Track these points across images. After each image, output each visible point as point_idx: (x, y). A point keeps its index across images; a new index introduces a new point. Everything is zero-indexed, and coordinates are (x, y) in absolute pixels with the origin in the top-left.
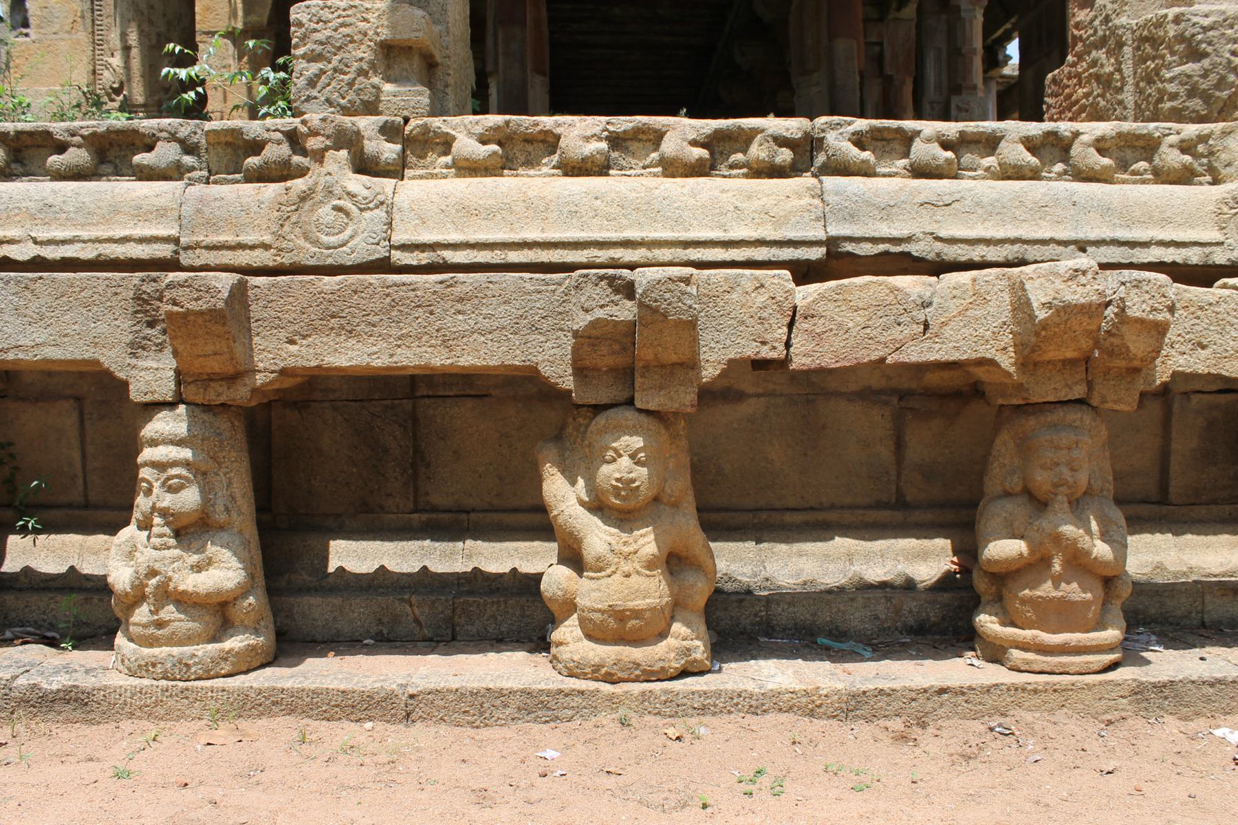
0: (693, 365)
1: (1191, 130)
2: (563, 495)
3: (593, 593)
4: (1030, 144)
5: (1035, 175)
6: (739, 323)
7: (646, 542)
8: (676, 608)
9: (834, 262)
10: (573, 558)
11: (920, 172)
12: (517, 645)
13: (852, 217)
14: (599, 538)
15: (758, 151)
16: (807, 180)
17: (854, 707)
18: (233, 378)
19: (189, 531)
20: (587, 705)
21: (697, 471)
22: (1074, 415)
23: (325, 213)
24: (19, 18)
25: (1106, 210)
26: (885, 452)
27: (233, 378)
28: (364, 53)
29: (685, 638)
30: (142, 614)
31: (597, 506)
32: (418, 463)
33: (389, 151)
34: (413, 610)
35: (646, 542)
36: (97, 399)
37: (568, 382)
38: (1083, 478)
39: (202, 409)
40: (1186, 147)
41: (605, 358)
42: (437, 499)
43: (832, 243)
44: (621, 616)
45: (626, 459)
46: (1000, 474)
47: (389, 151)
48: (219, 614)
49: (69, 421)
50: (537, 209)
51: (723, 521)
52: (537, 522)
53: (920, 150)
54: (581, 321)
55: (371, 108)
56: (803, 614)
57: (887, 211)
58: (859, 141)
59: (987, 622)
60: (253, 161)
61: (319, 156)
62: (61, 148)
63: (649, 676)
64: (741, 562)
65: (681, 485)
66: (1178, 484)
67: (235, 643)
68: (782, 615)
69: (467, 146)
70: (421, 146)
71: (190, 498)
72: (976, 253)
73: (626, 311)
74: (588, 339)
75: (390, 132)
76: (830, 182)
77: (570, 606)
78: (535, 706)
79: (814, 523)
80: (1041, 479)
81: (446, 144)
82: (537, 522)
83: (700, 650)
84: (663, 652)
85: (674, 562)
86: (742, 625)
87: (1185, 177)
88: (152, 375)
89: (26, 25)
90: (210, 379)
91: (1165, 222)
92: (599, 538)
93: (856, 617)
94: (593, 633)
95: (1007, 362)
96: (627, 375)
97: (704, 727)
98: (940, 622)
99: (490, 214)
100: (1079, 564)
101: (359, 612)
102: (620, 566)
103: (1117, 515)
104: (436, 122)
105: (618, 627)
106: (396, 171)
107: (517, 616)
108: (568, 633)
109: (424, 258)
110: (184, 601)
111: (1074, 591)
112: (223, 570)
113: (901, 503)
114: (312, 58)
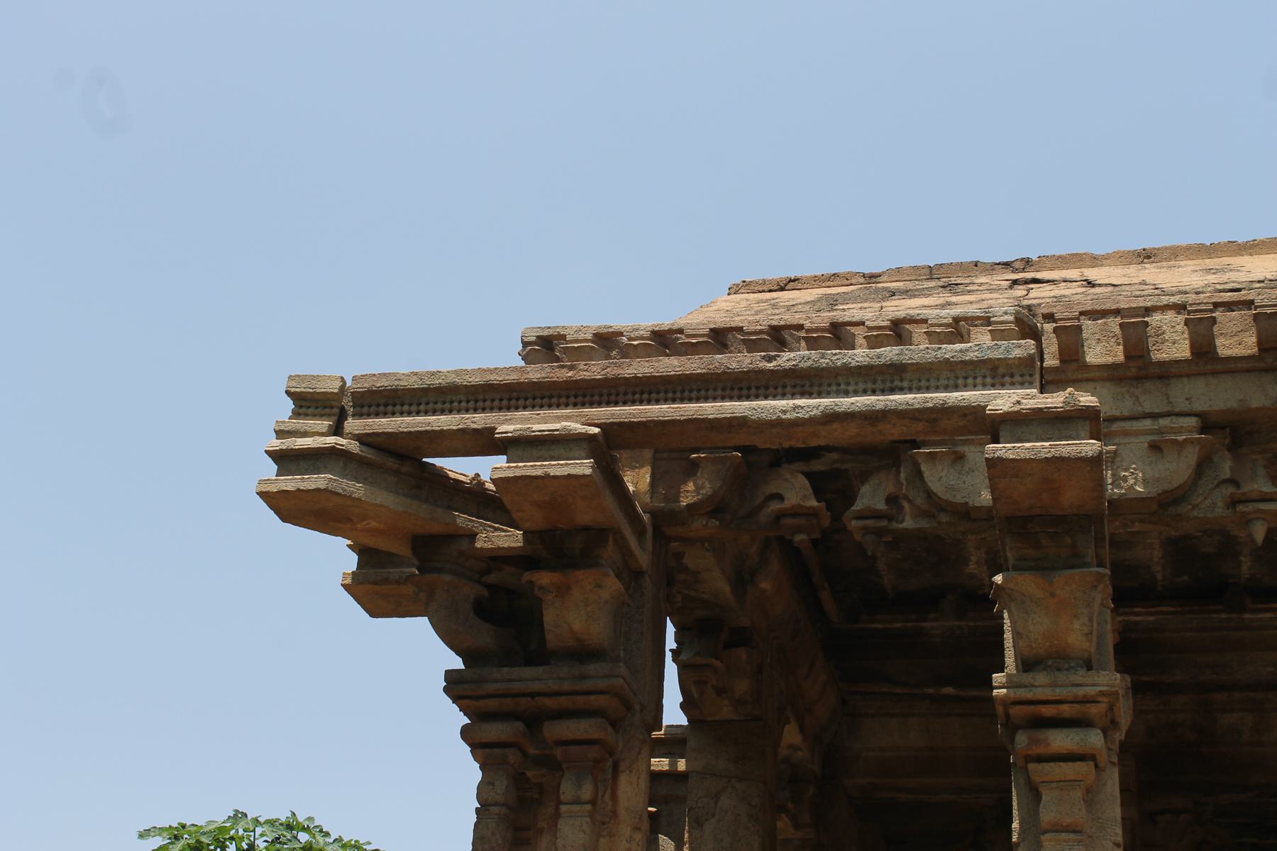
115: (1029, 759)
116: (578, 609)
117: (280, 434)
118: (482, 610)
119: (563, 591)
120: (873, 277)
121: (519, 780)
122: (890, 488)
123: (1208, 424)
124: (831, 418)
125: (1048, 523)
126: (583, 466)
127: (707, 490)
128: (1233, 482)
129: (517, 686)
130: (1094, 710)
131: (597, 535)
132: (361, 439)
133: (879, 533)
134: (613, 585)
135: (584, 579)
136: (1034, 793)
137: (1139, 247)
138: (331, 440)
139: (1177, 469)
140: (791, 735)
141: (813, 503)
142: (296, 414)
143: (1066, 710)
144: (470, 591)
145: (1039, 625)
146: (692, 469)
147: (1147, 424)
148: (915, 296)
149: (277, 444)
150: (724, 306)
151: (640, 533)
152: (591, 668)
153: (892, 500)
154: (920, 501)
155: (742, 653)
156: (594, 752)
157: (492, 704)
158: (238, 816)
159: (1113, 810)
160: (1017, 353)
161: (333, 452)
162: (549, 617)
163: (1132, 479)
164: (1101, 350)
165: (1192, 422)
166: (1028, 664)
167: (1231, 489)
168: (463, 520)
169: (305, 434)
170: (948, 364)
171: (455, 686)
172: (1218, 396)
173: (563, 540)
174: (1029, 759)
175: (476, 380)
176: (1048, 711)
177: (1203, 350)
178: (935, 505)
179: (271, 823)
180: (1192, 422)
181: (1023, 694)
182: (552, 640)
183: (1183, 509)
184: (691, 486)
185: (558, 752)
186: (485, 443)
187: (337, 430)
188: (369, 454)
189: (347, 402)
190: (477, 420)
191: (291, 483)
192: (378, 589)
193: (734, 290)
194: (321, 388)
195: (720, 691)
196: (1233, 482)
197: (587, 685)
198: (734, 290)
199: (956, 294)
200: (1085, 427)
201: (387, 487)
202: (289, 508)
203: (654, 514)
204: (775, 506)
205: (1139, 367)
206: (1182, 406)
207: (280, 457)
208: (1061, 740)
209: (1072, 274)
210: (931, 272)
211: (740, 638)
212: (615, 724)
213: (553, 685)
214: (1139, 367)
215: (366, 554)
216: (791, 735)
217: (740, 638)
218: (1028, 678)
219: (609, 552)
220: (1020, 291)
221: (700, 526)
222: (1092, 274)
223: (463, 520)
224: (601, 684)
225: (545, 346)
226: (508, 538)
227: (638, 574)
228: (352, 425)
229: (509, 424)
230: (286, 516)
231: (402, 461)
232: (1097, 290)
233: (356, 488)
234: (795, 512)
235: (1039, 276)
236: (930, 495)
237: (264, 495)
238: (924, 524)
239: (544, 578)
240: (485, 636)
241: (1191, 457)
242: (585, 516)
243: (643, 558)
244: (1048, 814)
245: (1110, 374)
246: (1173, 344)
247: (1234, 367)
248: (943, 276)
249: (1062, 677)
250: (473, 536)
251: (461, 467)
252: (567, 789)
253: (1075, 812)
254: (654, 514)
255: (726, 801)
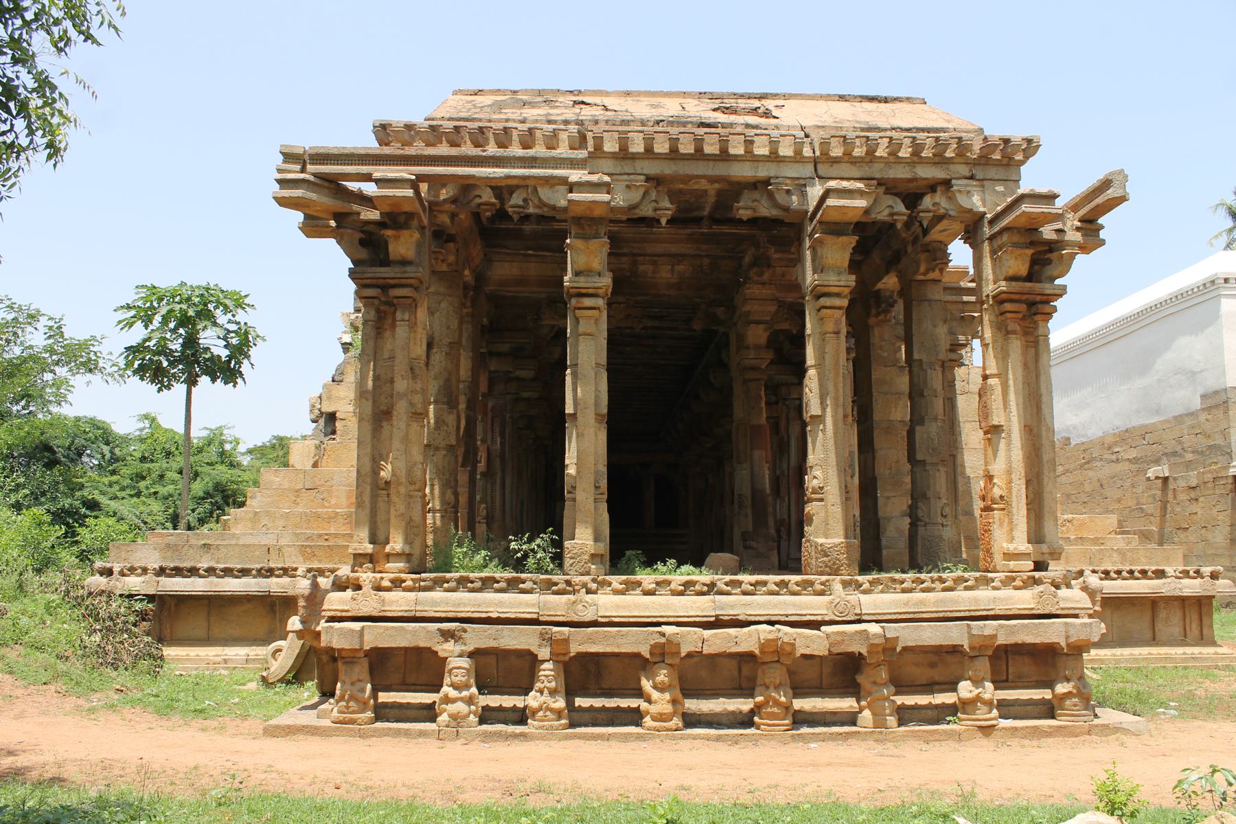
0: (679, 653)
1: (824, 578)
2: (646, 685)
3: (653, 709)
4: (776, 584)
5: (777, 594)
6: (690, 640)
7: (667, 696)
8: (674, 713)
9: (718, 623)
10: (649, 701)
11: (745, 593)
12: (1043, 378)
13: (722, 609)
14: (655, 695)
15: (698, 587)
16: (711, 597)
17: (718, 739)
18: (564, 654)
19: (553, 692)
20: (653, 737)
21: (680, 678)
22: (775, 665)
23: (580, 607)
24: (329, 430)
25: (795, 605)
26: (736, 673)
27: (564, 654)
28: (586, 557)
29: (677, 721)
30: (541, 714)
31: (655, 687)
32: (599, 675)
33: (594, 586)
34: (603, 716)
35: (667, 696)
36: (530, 661)
37: (648, 656)
38: (778, 681)
39: (556, 662)
40: (822, 584)
41: (658, 651)
42: (604, 686)
43: (717, 616)
44: (661, 714)
45: (662, 676)
46: (759, 681)
47: (594, 586)
48: (559, 714)
49: (494, 661)
50: (637, 606)
51: (688, 693)
52: (639, 693)
53: (745, 587)
54: (652, 642)
55: (588, 573)
56: (709, 719)
57: (732, 607)
58: (727, 584)
59: (756, 719)
60: (554, 588)
61: (578, 591)
62: (498, 582)
63: (670, 730)
64: (692, 705)
65: (676, 682)
66: (824, 683)
67: (563, 721)
68: (703, 719)
69: (616, 585)
70: (603, 584)
71: (553, 684)
72: (757, 619)
73: (663, 640)
74: (654, 647)
75: (594, 581)
76: (718, 597)
77: (648, 713)
78: (639, 737)
79: (714, 694)
80: (767, 681)
81: (610, 584)
82: (639, 693)
83: (680, 725)
84: (671, 724)
85: (674, 702)
86: (691, 721)
87: (822, 593)
88: (544, 653)
89: (334, 432)
90: (558, 655)
91: (811, 608)
92: (655, 695)
93: (724, 720)
94: (654, 719)
95: (757, 652)
96: (663, 654)
97: (681, 742)
98: (746, 721)
99: (624, 607)
100: (777, 703)
101: (587, 717)
102: (661, 702)
103: (791, 692)
104: (607, 578)
105: (660, 718)
106: (595, 592)
107: (635, 717)
108: (647, 721)
109: (606, 620)
110: (552, 710)
111: (775, 710)
112: (560, 703)
113: (741, 688)
114: (571, 558)
115: (576, 308)
116: (403, 245)
117: (280, 171)
118: (362, 243)
119: (397, 238)
120: (515, 92)
121: (378, 311)
122: (525, 195)
123: (649, 179)
124: (508, 177)
125: (586, 222)
126: (409, 193)
127: (451, 193)
128: (656, 201)
129: (378, 275)
130: (600, 291)
131: (411, 216)
132: (314, 175)
133: (519, 213)
134: (417, 235)
135: (405, 234)
136: (577, 320)
137: (625, 89)
138: (302, 176)
139: (635, 196)
140: (467, 272)
141: (494, 200)
142: (284, 162)
143: (590, 291)
144: (358, 235)
145: (582, 261)
146: (444, 185)
147: (626, 177)
148: (533, 107)
149: (279, 176)
150: (451, 103)
151: (424, 211)
152: (408, 269)
153: (525, 200)
154: (536, 201)
155: (451, 245)
156: (410, 301)
157: (368, 281)
158: (183, 284)
159: (604, 326)
160: (581, 156)
161: (303, 180)
162: (391, 248)
163: (620, 199)
164: (610, 146)
165: (643, 178)
166: (577, 274)
167: (654, 204)
168: (356, 207)
169: (290, 172)
170: (554, 159)
171: (353, 274)
172: (653, 168)
173: (396, 218)
174: (576, 308)
175: (363, 152)
176: (583, 291)
177: (649, 150)
178: (542, 204)
179: (199, 287)
180: (643, 178)
181: (576, 285)
182: (392, 257)
183: (637, 211)
184: (444, 191)
185: (395, 301)
186: (367, 178)
187: (303, 170)
188: (318, 181)
189: (307, 158)
190: (364, 169)
191: (287, 193)
192: (313, 227)
193: (455, 93)
194: (296, 151)
195: (443, 261)
196: (656, 201)
197: (407, 275)
198: (455, 93)
199: (552, 108)
200: (605, 189)
201: (323, 194)
202: (282, 202)
203: (430, 203)
204: (478, 200)
205: (624, 154)
206: (639, 171)
207: (279, 181)
208: (588, 302)
209: (597, 100)
210: (540, 93)
211: (451, 238)
212: (416, 289)
213: (393, 275)
214: (624, 154)
215: (307, 217)
216: (467, 272)
217: (451, 238)
218: (577, 279)
219: (415, 223)
220: (577, 109)
221: (448, 207)
222: (607, 101)
223: (356, 207)
224: (412, 275)
225: (383, 131)
226: (374, 215)
227: (423, 228)
228: (309, 167)
229: (380, 172)
230: (281, 205)
231: (331, 184)
232: (609, 113)
233: (312, 196)
234: (485, 204)
235: (586, 99)
236: (540, 199)
237: (275, 198)
238: (537, 211)
239: (389, 233)
240: (363, 254)
241: (642, 191)
242: (407, 208)
243: (426, 221)
244: (581, 329)
245: (613, 156)
246: (637, 147)
247: (659, 157)
248: (546, 97)
249: (590, 279)
250: (359, 214)
251: (353, 186)
252: (399, 315)
253: (592, 329)
254: (430, 203)
255: (443, 305)
